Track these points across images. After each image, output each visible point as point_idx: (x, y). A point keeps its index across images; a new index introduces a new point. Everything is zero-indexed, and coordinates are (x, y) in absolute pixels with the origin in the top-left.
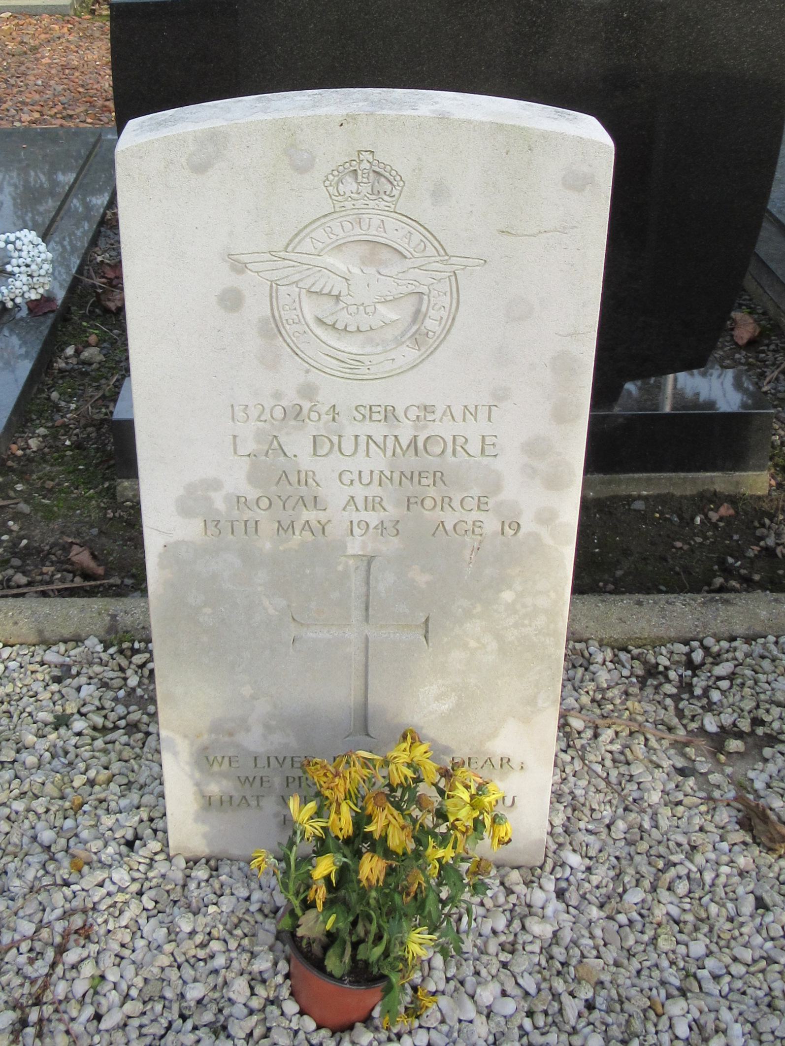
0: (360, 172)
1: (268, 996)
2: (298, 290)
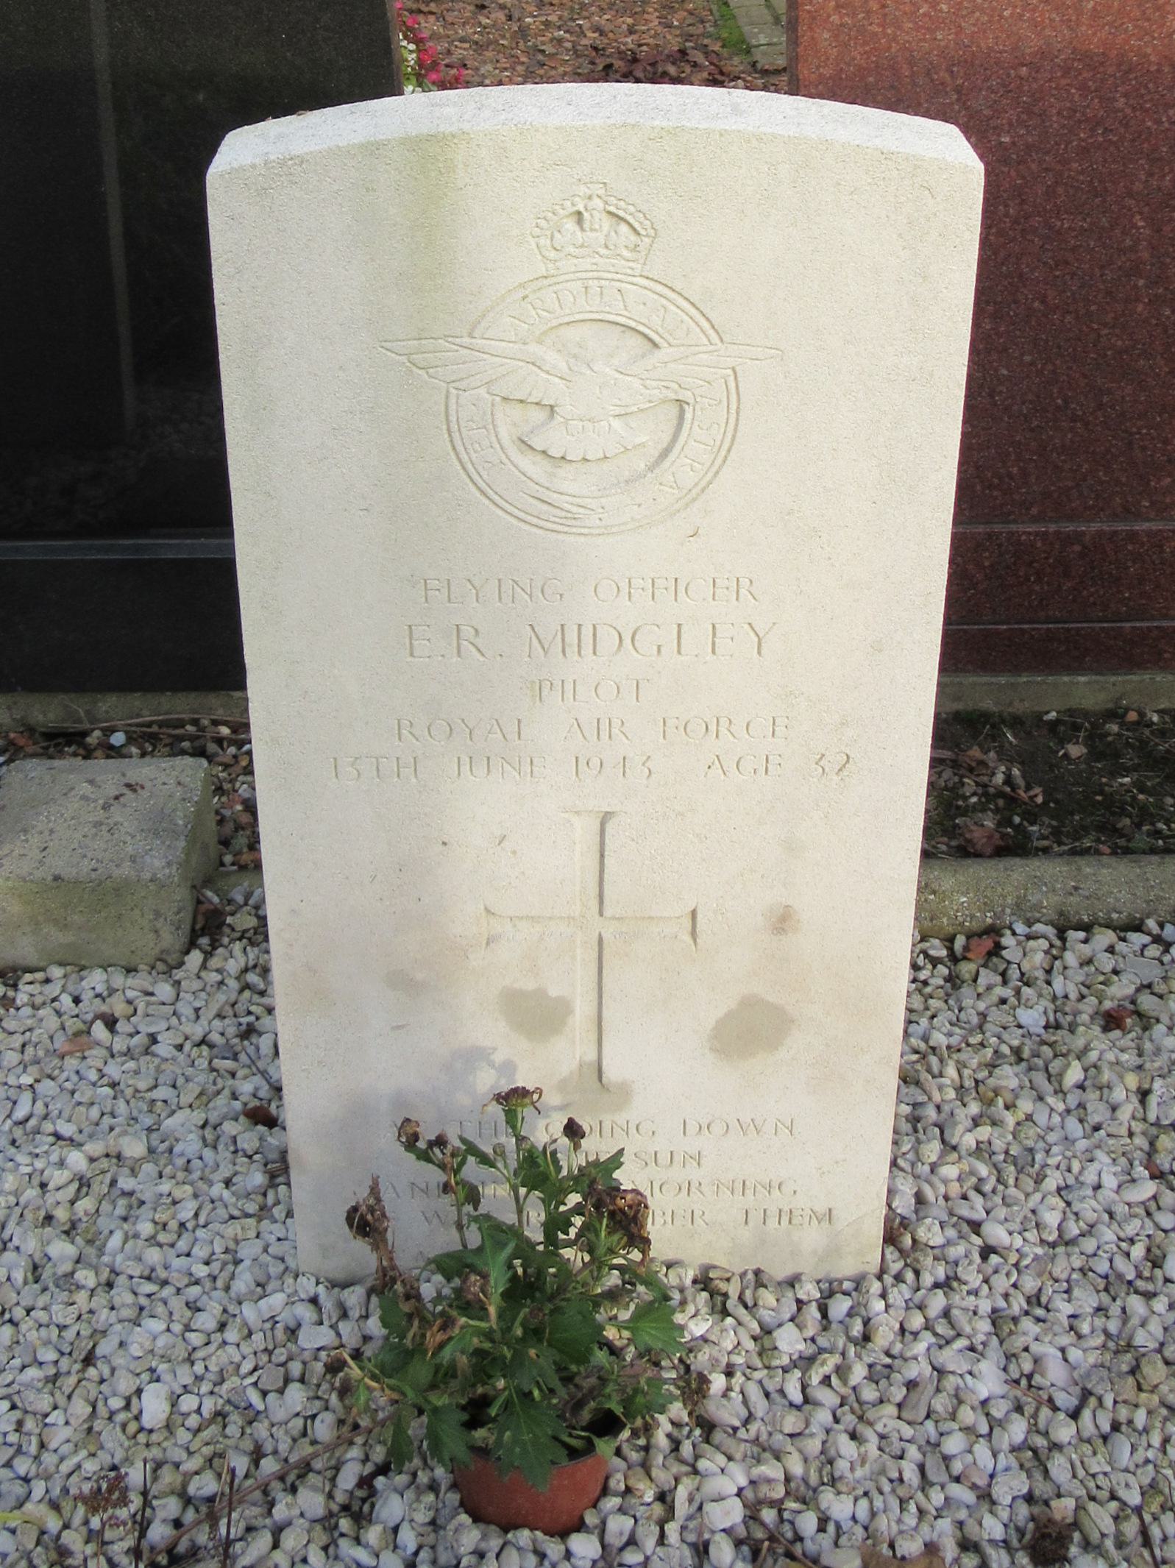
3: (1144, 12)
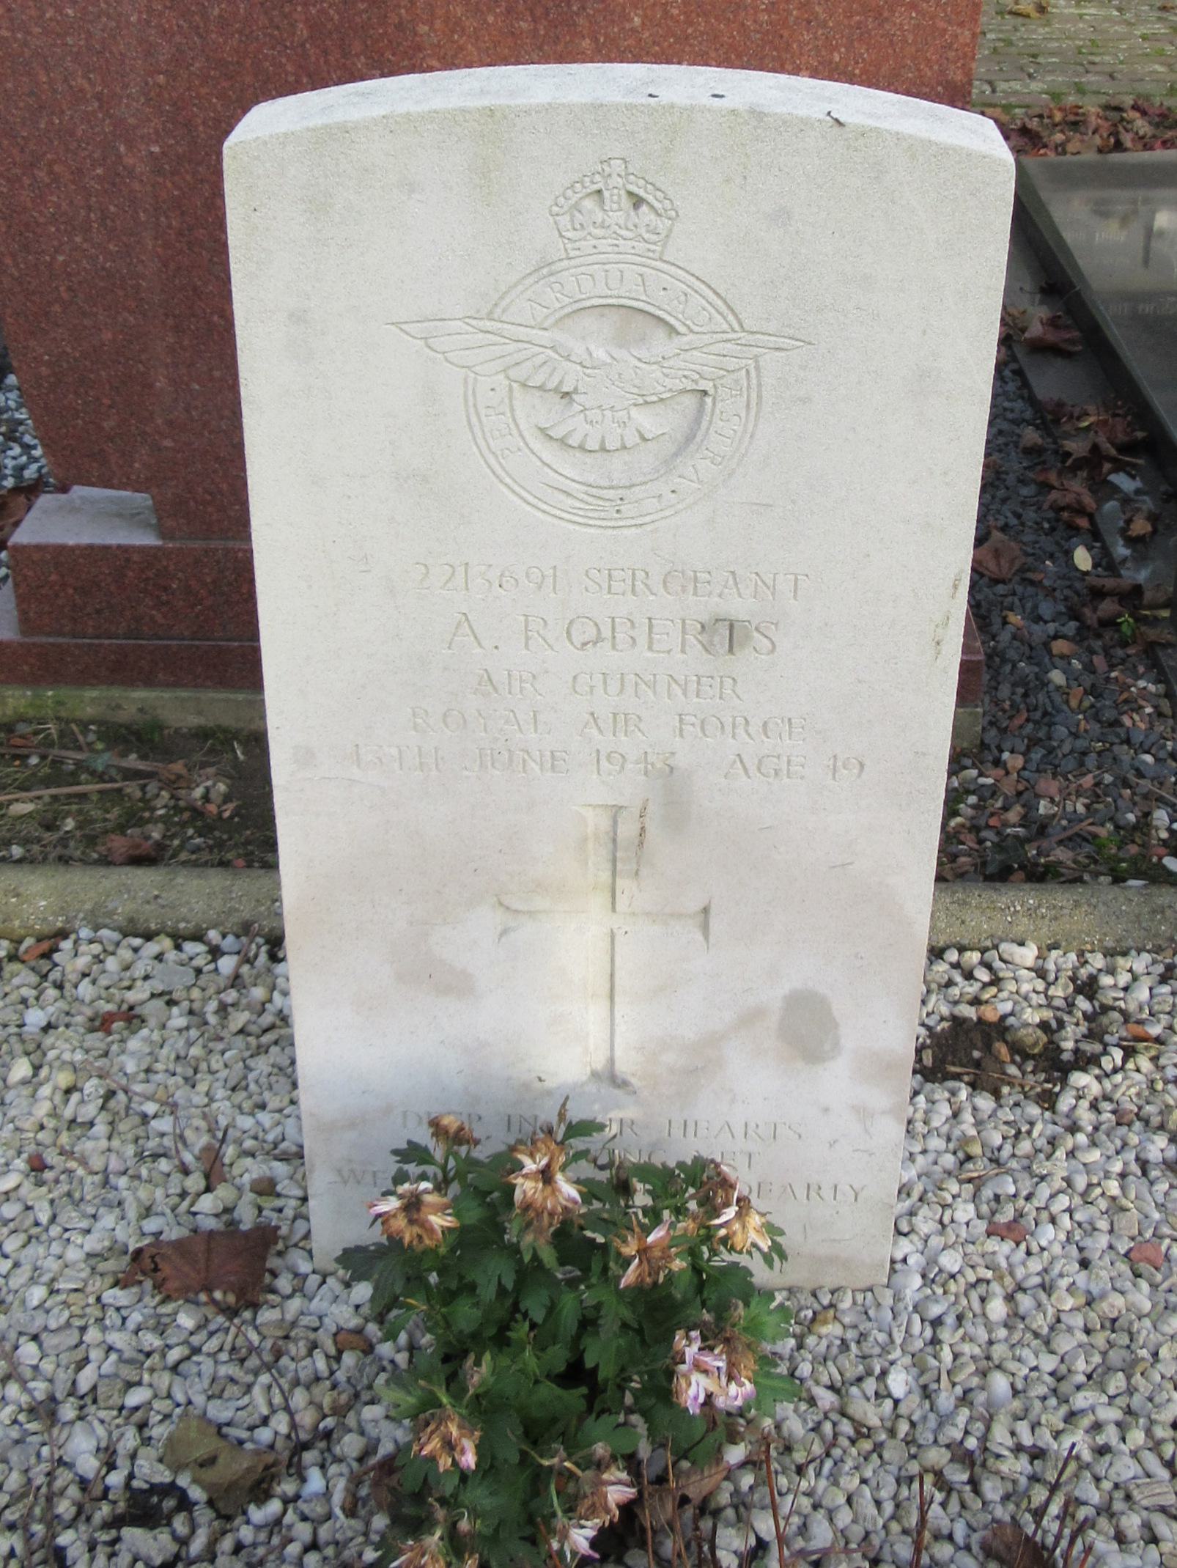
0: (606, 194)
1: (22, 1172)
2: (507, 382)
3: (271, 20)
